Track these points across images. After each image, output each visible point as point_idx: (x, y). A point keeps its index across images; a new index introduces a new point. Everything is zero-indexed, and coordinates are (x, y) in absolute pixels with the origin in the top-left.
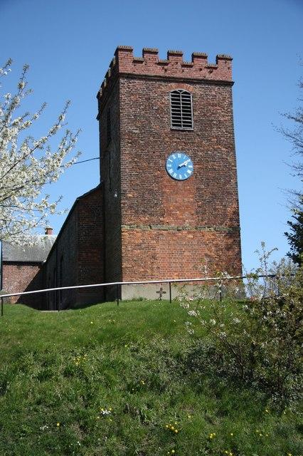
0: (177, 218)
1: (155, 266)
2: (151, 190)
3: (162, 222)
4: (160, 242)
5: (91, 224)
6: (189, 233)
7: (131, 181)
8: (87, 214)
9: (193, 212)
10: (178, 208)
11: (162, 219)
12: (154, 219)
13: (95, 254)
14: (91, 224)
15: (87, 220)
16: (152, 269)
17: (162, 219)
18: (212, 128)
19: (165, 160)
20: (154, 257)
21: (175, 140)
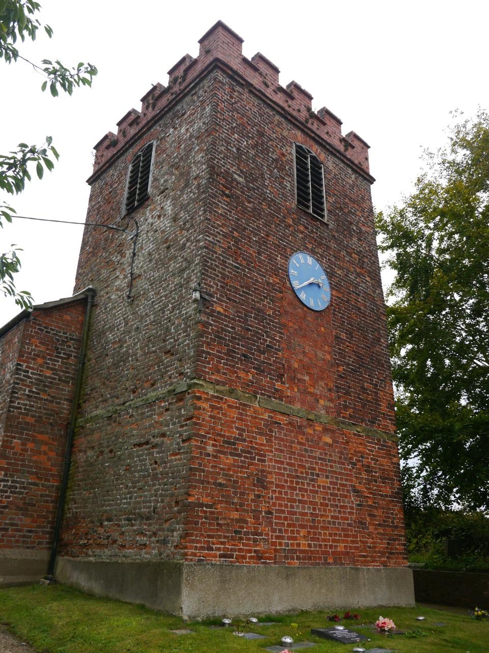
0: (305, 392)
1: (263, 507)
2: (259, 310)
3: (279, 395)
4: (275, 444)
5: (49, 374)
6: (326, 430)
7: (224, 276)
8: (43, 348)
9: (331, 385)
10: (306, 368)
11: (278, 385)
12: (265, 381)
13: (44, 448)
14: (49, 374)
15: (40, 361)
16: (256, 514)
17: (278, 385)
18: (351, 236)
19: (287, 258)
20: (261, 483)
21: (302, 228)
